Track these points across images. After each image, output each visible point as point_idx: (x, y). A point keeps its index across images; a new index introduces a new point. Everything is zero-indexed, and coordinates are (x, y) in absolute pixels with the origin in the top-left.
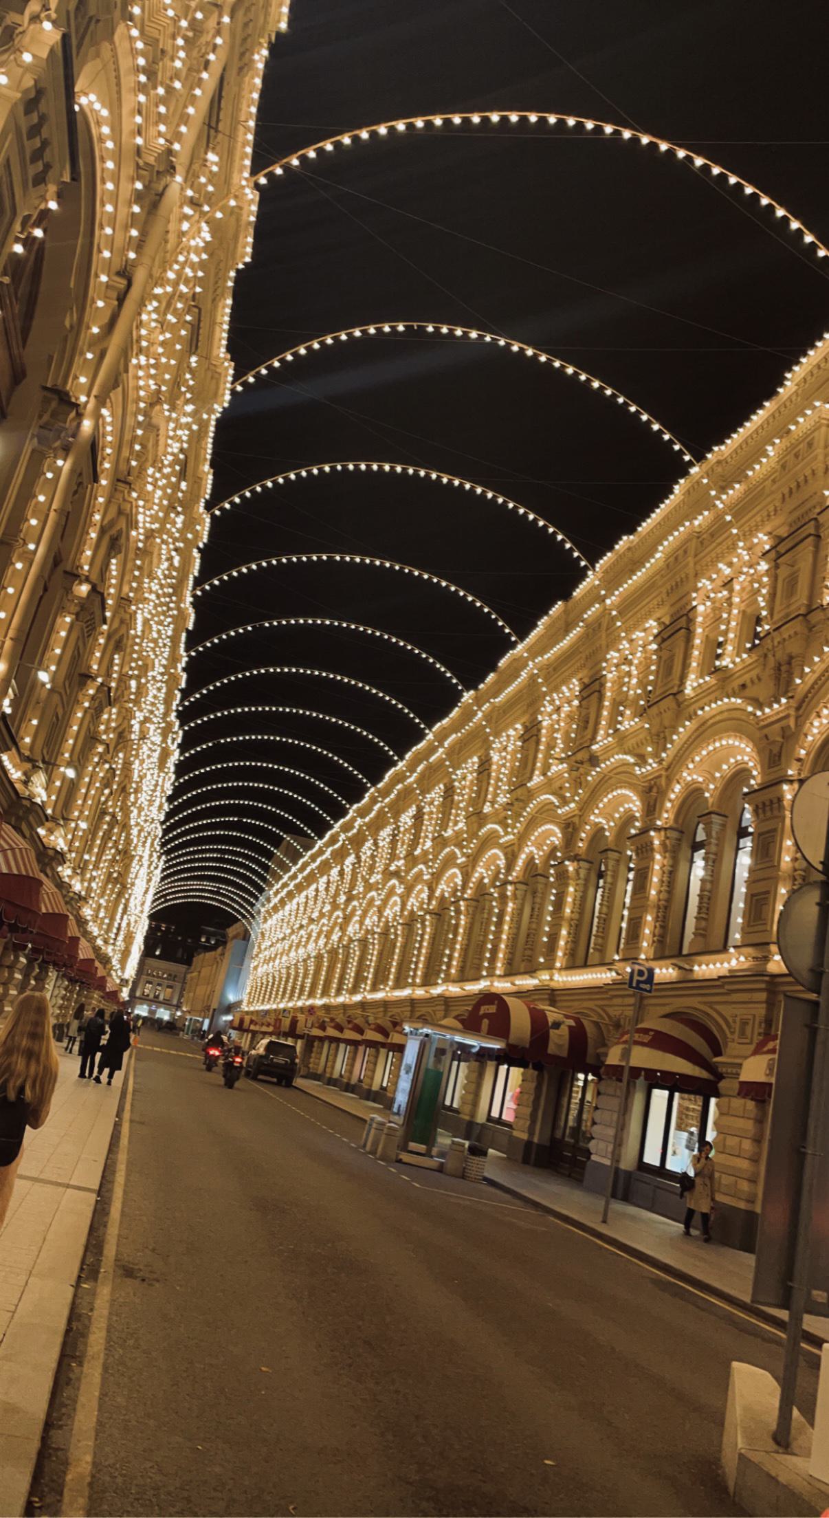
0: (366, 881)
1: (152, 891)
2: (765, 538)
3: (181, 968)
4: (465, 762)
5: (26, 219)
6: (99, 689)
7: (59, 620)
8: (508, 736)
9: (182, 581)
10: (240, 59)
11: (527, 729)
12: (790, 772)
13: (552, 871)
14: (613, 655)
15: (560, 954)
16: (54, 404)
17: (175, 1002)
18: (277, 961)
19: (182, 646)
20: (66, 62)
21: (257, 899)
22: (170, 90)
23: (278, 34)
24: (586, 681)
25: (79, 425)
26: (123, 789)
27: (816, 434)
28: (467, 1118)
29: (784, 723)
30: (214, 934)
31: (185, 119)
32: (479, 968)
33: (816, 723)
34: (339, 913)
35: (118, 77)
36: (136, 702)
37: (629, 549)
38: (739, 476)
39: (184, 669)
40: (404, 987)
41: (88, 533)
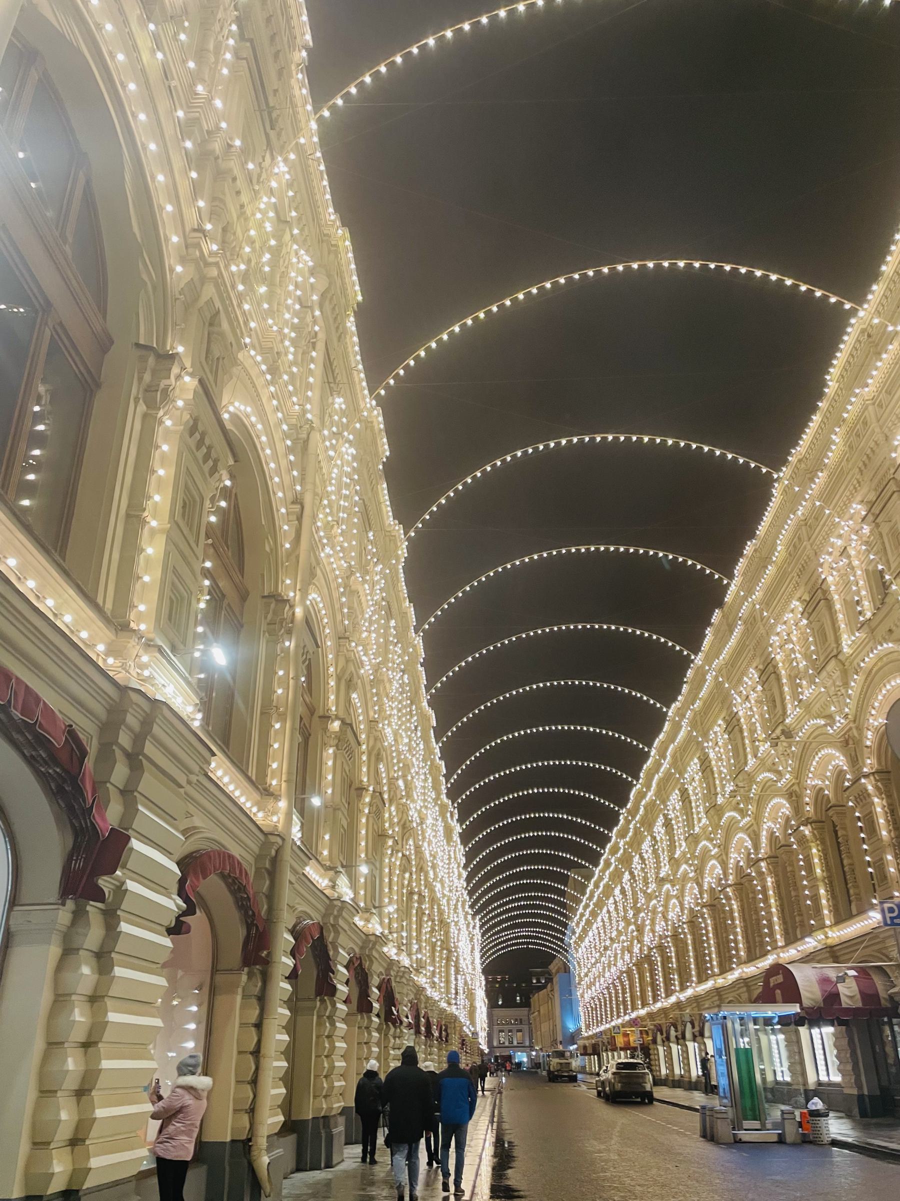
0: (645, 892)
1: (477, 948)
2: (859, 507)
3: (523, 1012)
4: (688, 764)
5: (213, 497)
6: (372, 797)
7: (325, 754)
8: (715, 733)
9: (416, 692)
10: (337, 331)
13: (792, 840)
14: (774, 638)
15: (826, 912)
16: (273, 606)
17: (527, 1044)
18: (597, 984)
19: (433, 740)
20: (208, 394)
21: (564, 934)
22: (292, 375)
23: (358, 304)
24: (761, 667)
25: (294, 614)
26: (421, 869)
27: (866, 413)
30: (542, 974)
31: (309, 387)
32: (762, 944)
34: (632, 927)
35: (253, 382)
36: (409, 796)
37: (755, 550)
38: (820, 466)
40: (707, 980)
41: (328, 684)
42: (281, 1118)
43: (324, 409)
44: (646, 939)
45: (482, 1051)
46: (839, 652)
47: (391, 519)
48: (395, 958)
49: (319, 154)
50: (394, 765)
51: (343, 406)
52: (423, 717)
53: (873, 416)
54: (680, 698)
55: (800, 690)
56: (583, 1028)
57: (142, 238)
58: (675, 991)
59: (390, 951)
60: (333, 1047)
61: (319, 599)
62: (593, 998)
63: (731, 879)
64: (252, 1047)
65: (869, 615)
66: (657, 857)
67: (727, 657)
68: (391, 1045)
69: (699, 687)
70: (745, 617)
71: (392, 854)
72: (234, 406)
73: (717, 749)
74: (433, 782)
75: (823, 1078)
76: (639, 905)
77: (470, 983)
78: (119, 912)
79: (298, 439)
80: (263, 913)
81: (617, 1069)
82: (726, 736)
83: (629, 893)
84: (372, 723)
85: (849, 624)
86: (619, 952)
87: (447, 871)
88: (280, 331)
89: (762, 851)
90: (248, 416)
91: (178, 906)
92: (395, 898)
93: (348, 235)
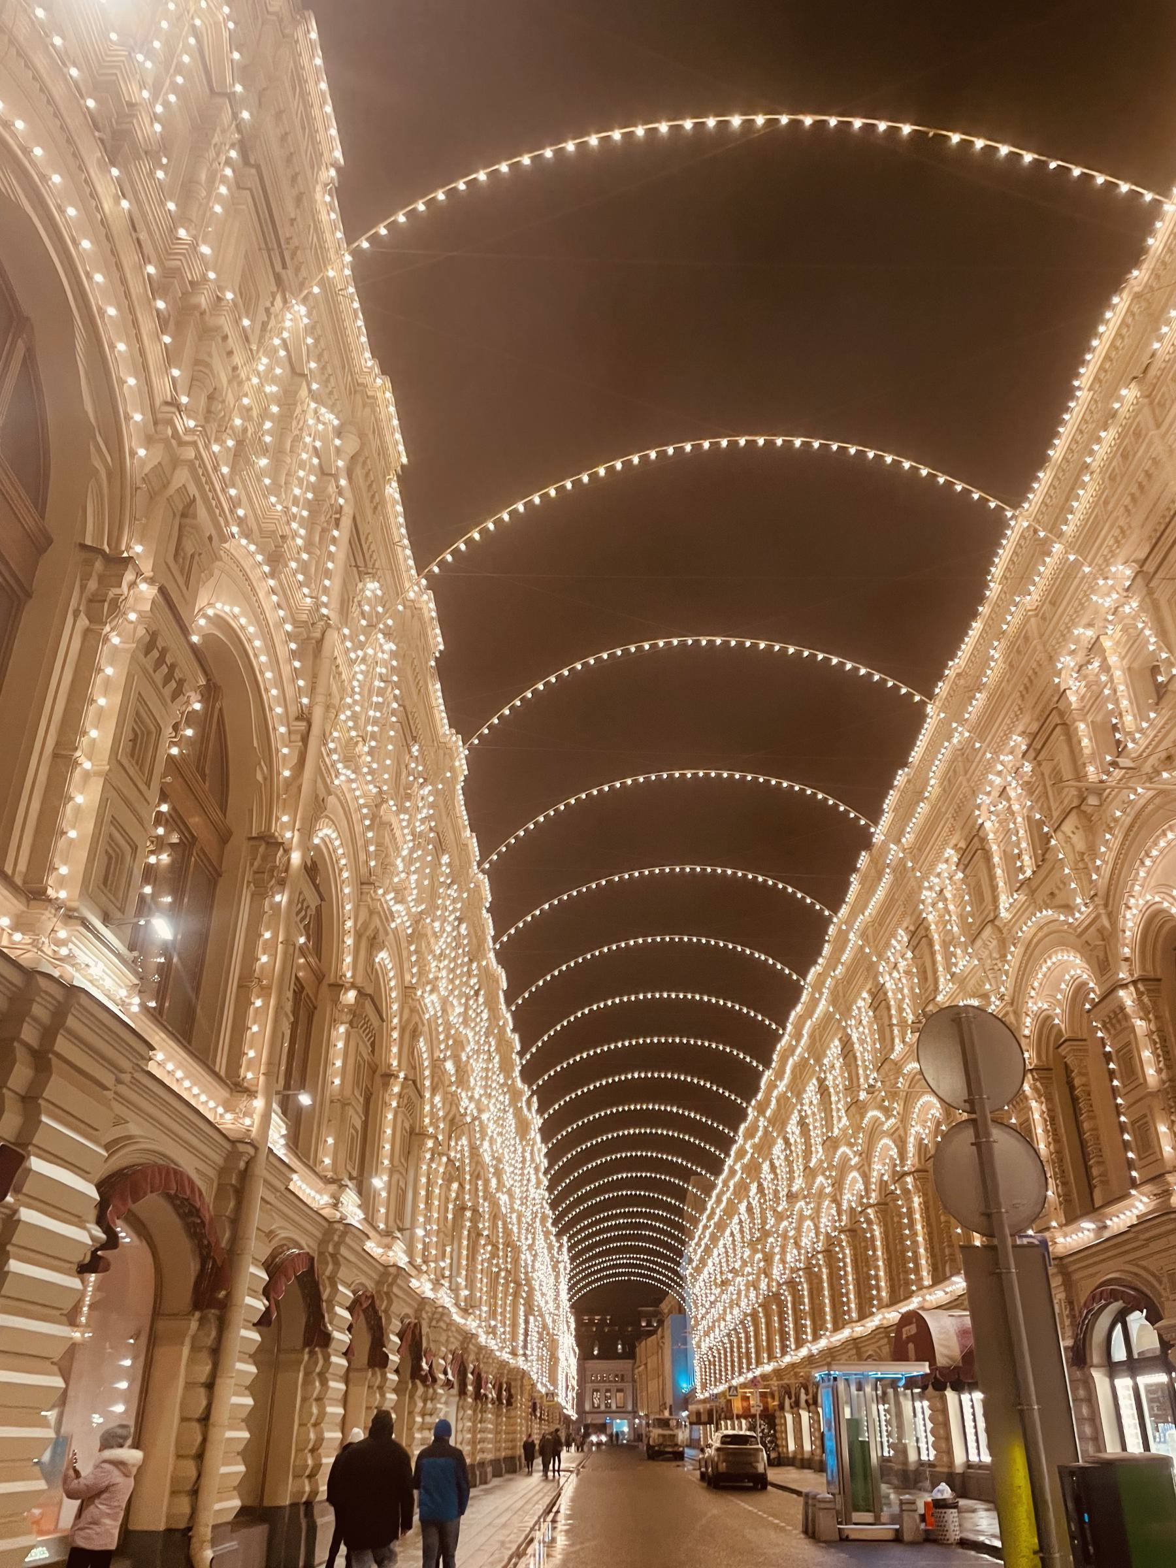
2: (1020, 739)
3: (625, 1365)
4: (828, 1047)
6: (403, 1086)
7: (334, 1033)
8: (859, 1008)
11: (874, 996)
12: (1121, 976)
16: (262, 849)
17: (630, 1408)
18: (717, 1330)
20: (172, 606)
21: (678, 1264)
24: (912, 928)
25: (289, 860)
28: (945, 1470)
29: (1097, 925)
31: (328, 574)
32: (908, 1283)
33: (1128, 916)
34: (759, 1256)
37: (909, 781)
39: (513, 1030)
41: (344, 942)
42: (236, 1503)
43: (346, 603)
44: (775, 1271)
45: (567, 1417)
46: (996, 917)
47: (447, 727)
48: (429, 1294)
49: (352, 290)
50: (440, 1043)
51: (379, 593)
52: (487, 976)
53: (1035, 631)
54: (820, 961)
55: (954, 960)
56: (699, 1387)
57: (97, 418)
58: (807, 1341)
59: (423, 1286)
60: (322, 1414)
61: (334, 836)
62: (711, 1349)
63: (874, 1197)
64: (199, 1411)
65: (1029, 873)
66: (790, 1164)
67: (874, 913)
68: (418, 1409)
69: (842, 950)
70: (894, 864)
71: (432, 1159)
72: (214, 607)
73: (861, 1029)
74: (501, 1062)
75: (974, 1458)
76: (767, 1227)
77: (551, 1325)
78: (9, 1248)
79: (309, 638)
80: (223, 1245)
81: (722, 1443)
82: (871, 1013)
83: (757, 1211)
84: (408, 991)
85: (1009, 881)
86: (743, 1288)
87: (518, 1178)
88: (286, 510)
89: (909, 1162)
90: (235, 617)
91: (93, 1238)
92: (436, 1215)
93: (389, 385)
